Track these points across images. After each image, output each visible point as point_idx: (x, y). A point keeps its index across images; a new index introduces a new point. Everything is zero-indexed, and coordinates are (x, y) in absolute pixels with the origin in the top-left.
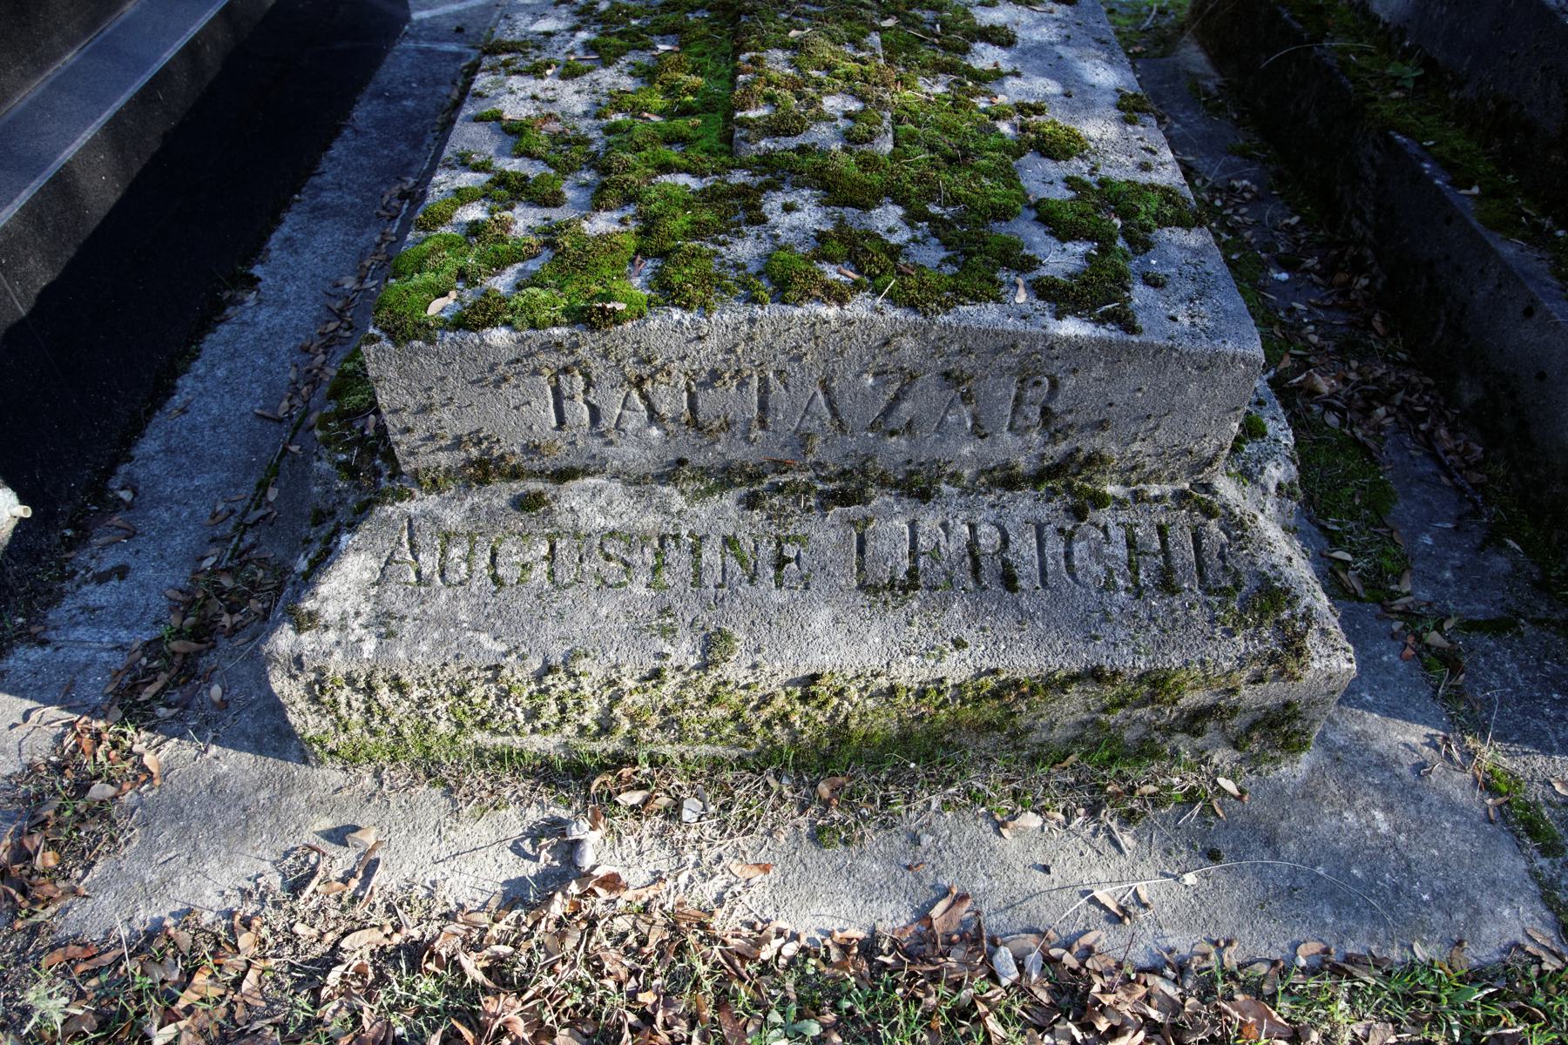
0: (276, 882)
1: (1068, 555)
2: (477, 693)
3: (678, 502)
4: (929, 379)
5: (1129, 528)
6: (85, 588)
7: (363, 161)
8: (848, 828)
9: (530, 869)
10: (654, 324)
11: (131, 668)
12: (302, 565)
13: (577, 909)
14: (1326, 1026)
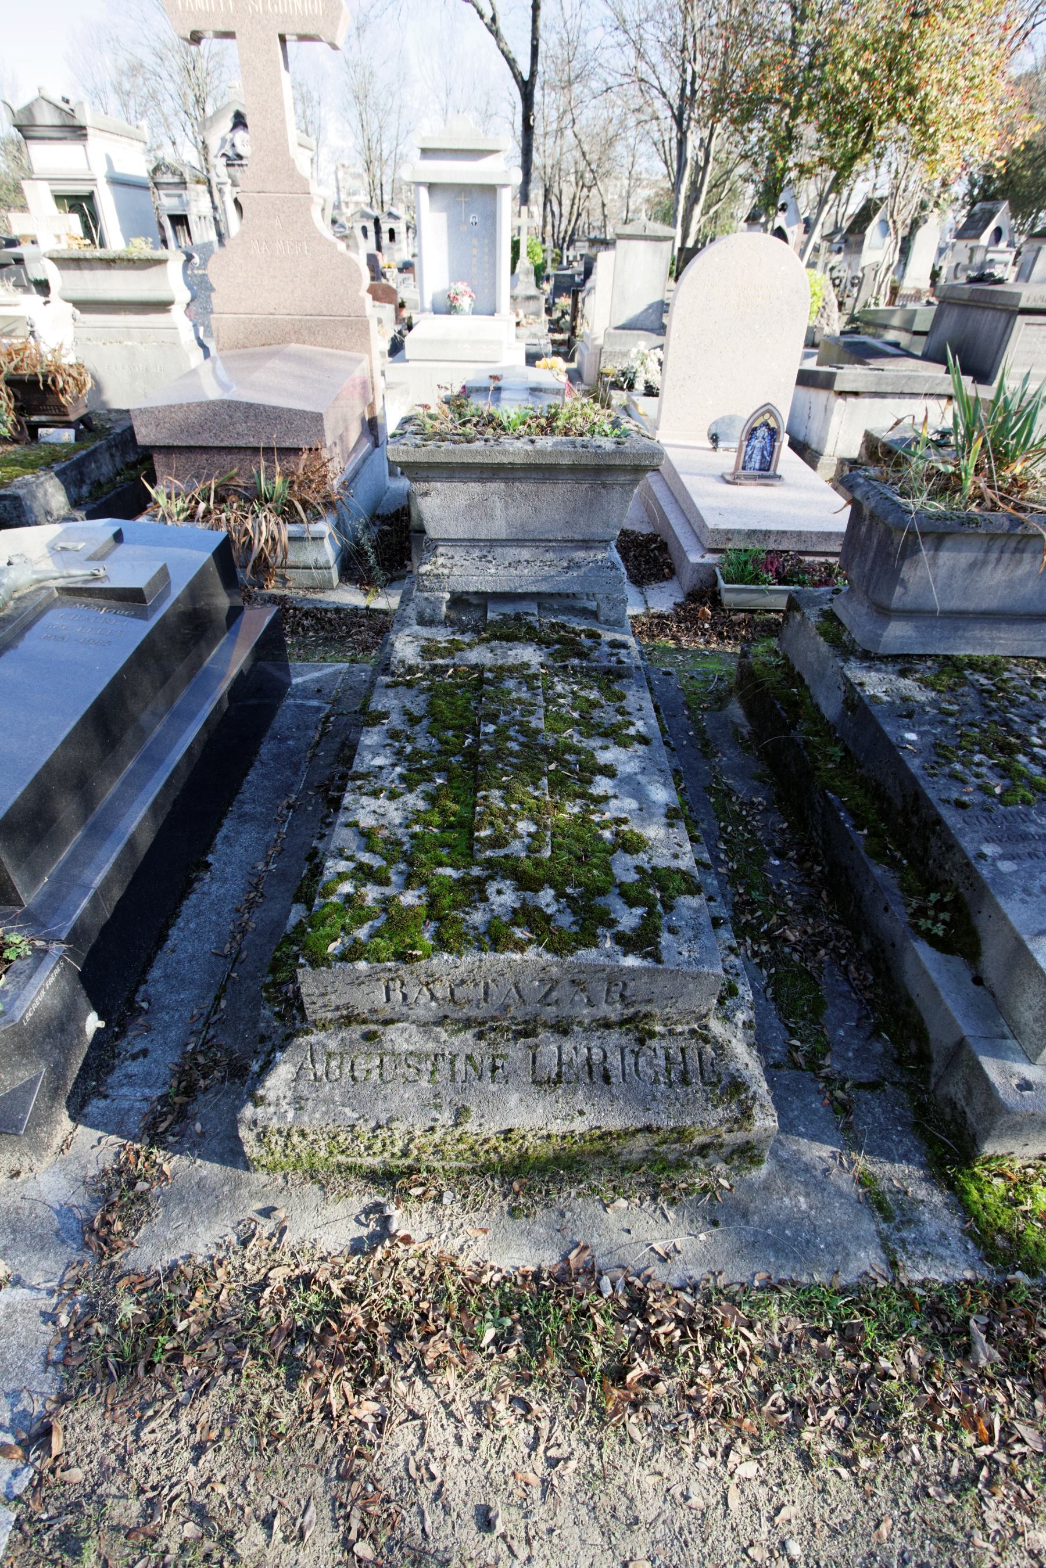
0: (234, 1239)
1: (636, 1064)
2: (341, 1138)
3: (444, 1036)
4: (565, 983)
5: (667, 1049)
6: (127, 1063)
7: (266, 783)
8: (528, 1208)
9: (365, 1232)
10: (435, 961)
11: (152, 1112)
12: (255, 1067)
13: (389, 1253)
14: (767, 1320)
